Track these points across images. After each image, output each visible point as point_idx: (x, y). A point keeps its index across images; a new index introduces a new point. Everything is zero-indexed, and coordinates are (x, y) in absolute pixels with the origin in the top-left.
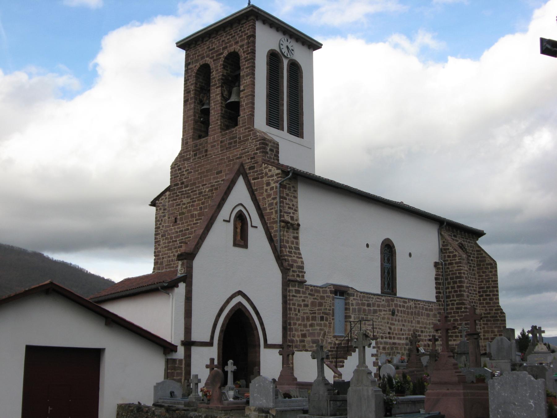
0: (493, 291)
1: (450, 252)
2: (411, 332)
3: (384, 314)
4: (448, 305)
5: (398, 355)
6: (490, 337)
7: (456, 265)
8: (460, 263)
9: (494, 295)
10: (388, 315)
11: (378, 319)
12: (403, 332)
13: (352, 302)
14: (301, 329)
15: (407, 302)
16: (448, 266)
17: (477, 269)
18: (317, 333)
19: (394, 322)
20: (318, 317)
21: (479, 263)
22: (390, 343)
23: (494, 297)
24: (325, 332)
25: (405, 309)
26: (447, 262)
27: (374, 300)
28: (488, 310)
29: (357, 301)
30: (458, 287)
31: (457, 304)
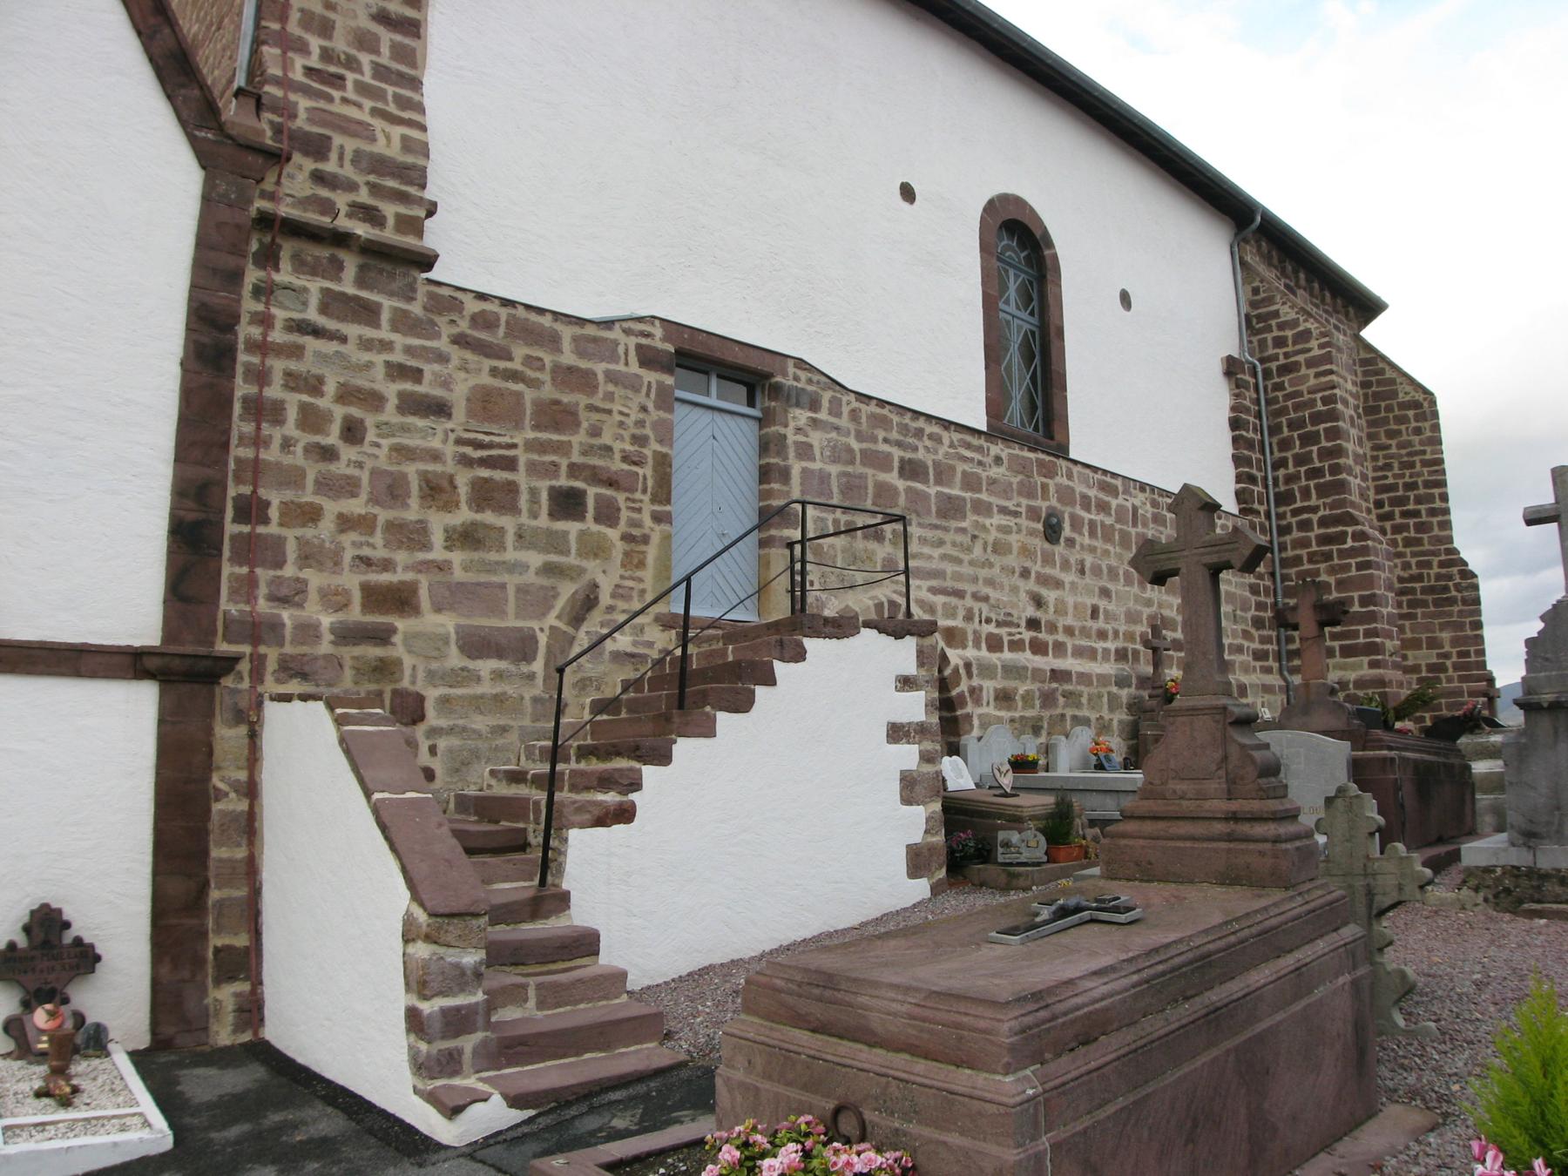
0: (1431, 498)
1: (1281, 327)
2: (1143, 628)
3: (1005, 530)
4: (1284, 530)
5: (1078, 729)
6: (1423, 663)
7: (1312, 372)
8: (1327, 358)
9: (1433, 512)
10: (1027, 533)
11: (969, 550)
12: (1101, 623)
13: (801, 438)
14: (366, 552)
15: (1121, 489)
16: (1277, 380)
17: (1365, 424)
18: (520, 590)
19: (1056, 572)
20: (534, 492)
21: (1371, 403)
22: (1037, 674)
23: (1435, 520)
24: (595, 586)
25: (1109, 521)
26: (1274, 365)
27: (944, 449)
28: (1414, 567)
29: (834, 435)
30: (1325, 454)
31: (1323, 522)
